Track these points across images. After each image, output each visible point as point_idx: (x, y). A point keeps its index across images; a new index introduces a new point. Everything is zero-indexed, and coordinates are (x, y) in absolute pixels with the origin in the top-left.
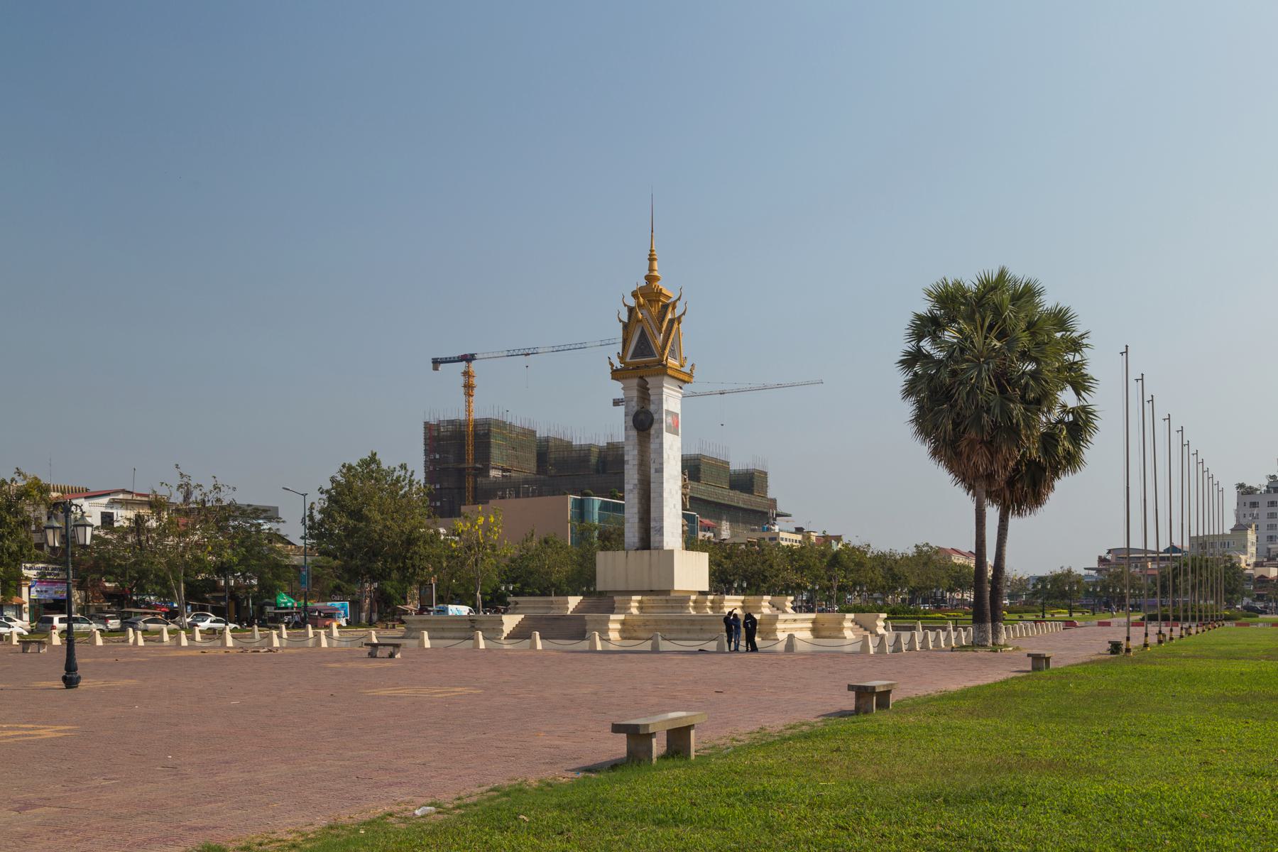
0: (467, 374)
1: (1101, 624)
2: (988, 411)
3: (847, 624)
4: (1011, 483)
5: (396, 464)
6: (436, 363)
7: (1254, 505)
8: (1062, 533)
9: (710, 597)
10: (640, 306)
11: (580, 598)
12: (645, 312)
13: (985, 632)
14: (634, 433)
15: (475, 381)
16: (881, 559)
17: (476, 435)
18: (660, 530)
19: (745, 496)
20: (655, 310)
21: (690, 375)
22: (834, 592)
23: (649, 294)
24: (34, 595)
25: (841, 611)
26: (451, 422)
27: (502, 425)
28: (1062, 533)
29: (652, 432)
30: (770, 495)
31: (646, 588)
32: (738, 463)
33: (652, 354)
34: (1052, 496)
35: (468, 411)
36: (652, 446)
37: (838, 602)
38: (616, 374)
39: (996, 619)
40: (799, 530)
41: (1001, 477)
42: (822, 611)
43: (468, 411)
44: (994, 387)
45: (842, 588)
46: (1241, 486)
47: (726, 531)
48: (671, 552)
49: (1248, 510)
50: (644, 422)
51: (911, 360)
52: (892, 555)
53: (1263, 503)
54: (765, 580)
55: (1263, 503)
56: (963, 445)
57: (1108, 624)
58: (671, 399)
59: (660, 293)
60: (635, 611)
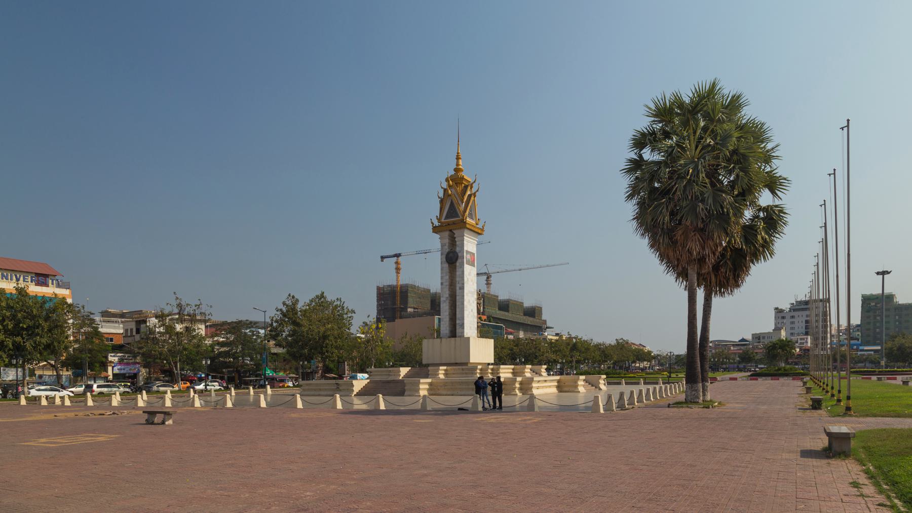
0: (397, 263)
1: (731, 379)
2: (703, 201)
3: (581, 383)
4: (716, 268)
5: (334, 298)
6: (383, 258)
7: (783, 318)
8: (744, 313)
9: (491, 367)
10: (450, 186)
11: (408, 369)
12: (453, 190)
13: (697, 391)
14: (446, 265)
15: (401, 266)
16: (598, 346)
17: (401, 292)
18: (462, 325)
19: (531, 319)
20: (459, 189)
21: (482, 230)
22: (574, 364)
23: (456, 180)
24: (116, 371)
25: (577, 374)
26: (389, 286)
27: (413, 287)
28: (744, 313)
29: (458, 264)
30: (544, 318)
31: (453, 361)
32: (527, 304)
33: (457, 216)
34: (748, 279)
35: (397, 280)
36: (458, 273)
37: (576, 369)
38: (436, 230)
39: (704, 380)
40: (557, 335)
41: (711, 261)
42: (567, 374)
43: (397, 280)
44: (702, 188)
45: (578, 362)
46: (776, 309)
47: (521, 335)
48: (468, 339)
49: (780, 321)
50: (452, 259)
51: (636, 165)
52: (604, 344)
53: (788, 317)
54: (536, 357)
55: (788, 317)
56: (679, 235)
57: (735, 379)
58: (470, 244)
59: (463, 178)
60: (442, 376)
